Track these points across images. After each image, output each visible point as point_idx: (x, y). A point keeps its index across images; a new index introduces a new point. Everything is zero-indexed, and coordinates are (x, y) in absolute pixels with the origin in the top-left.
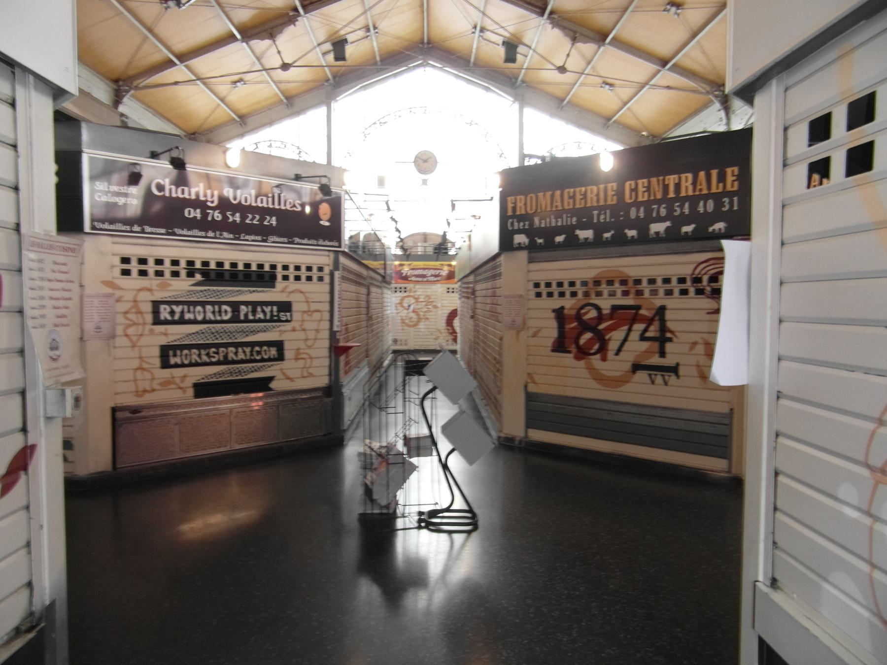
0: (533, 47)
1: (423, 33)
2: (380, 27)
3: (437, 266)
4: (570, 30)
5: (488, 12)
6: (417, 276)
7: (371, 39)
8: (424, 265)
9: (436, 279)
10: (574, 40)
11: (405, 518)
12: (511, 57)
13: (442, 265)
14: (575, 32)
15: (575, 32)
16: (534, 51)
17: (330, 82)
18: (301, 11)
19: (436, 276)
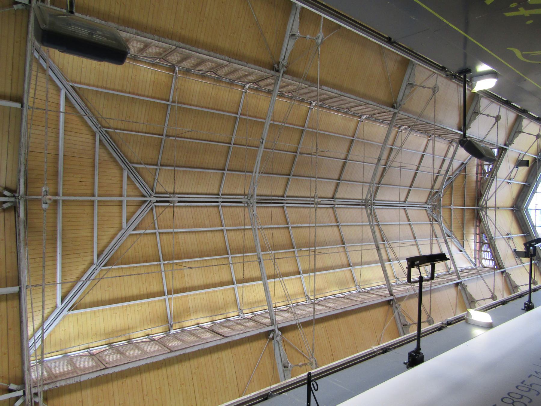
0: (524, 153)
4: (514, 135)
5: (365, 161)
7: (513, 237)
10: (520, 132)
11: (377, 160)
12: (526, 163)
14: (516, 132)
15: (516, 132)
16: (526, 153)
18: (503, 270)
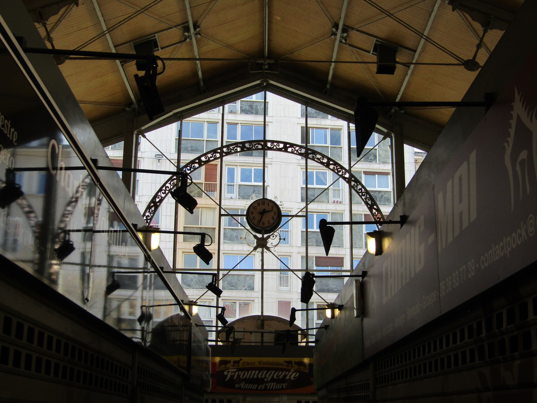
1: (263, 42)
2: (203, 25)
3: (282, 365)
6: (248, 381)
8: (260, 362)
9: (279, 386)
13: (290, 363)
17: (132, 106)
19: (278, 381)
